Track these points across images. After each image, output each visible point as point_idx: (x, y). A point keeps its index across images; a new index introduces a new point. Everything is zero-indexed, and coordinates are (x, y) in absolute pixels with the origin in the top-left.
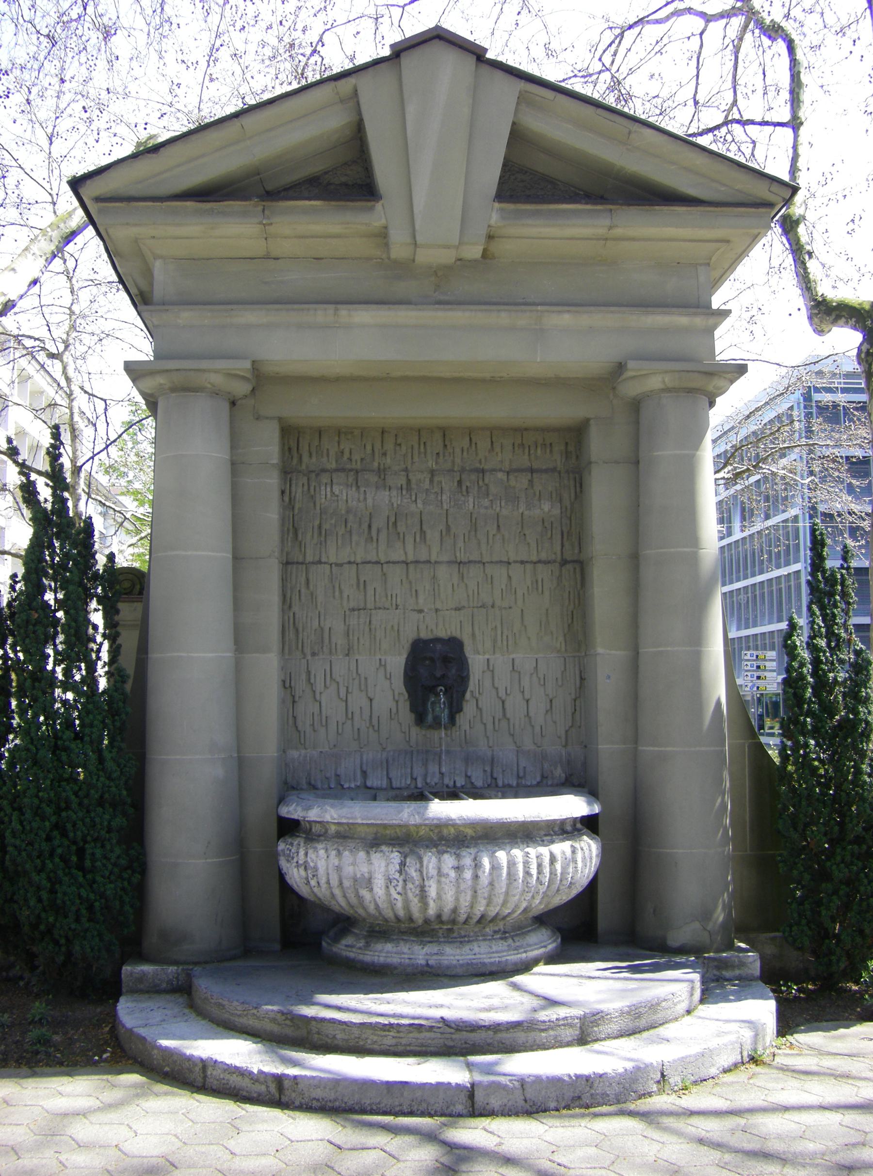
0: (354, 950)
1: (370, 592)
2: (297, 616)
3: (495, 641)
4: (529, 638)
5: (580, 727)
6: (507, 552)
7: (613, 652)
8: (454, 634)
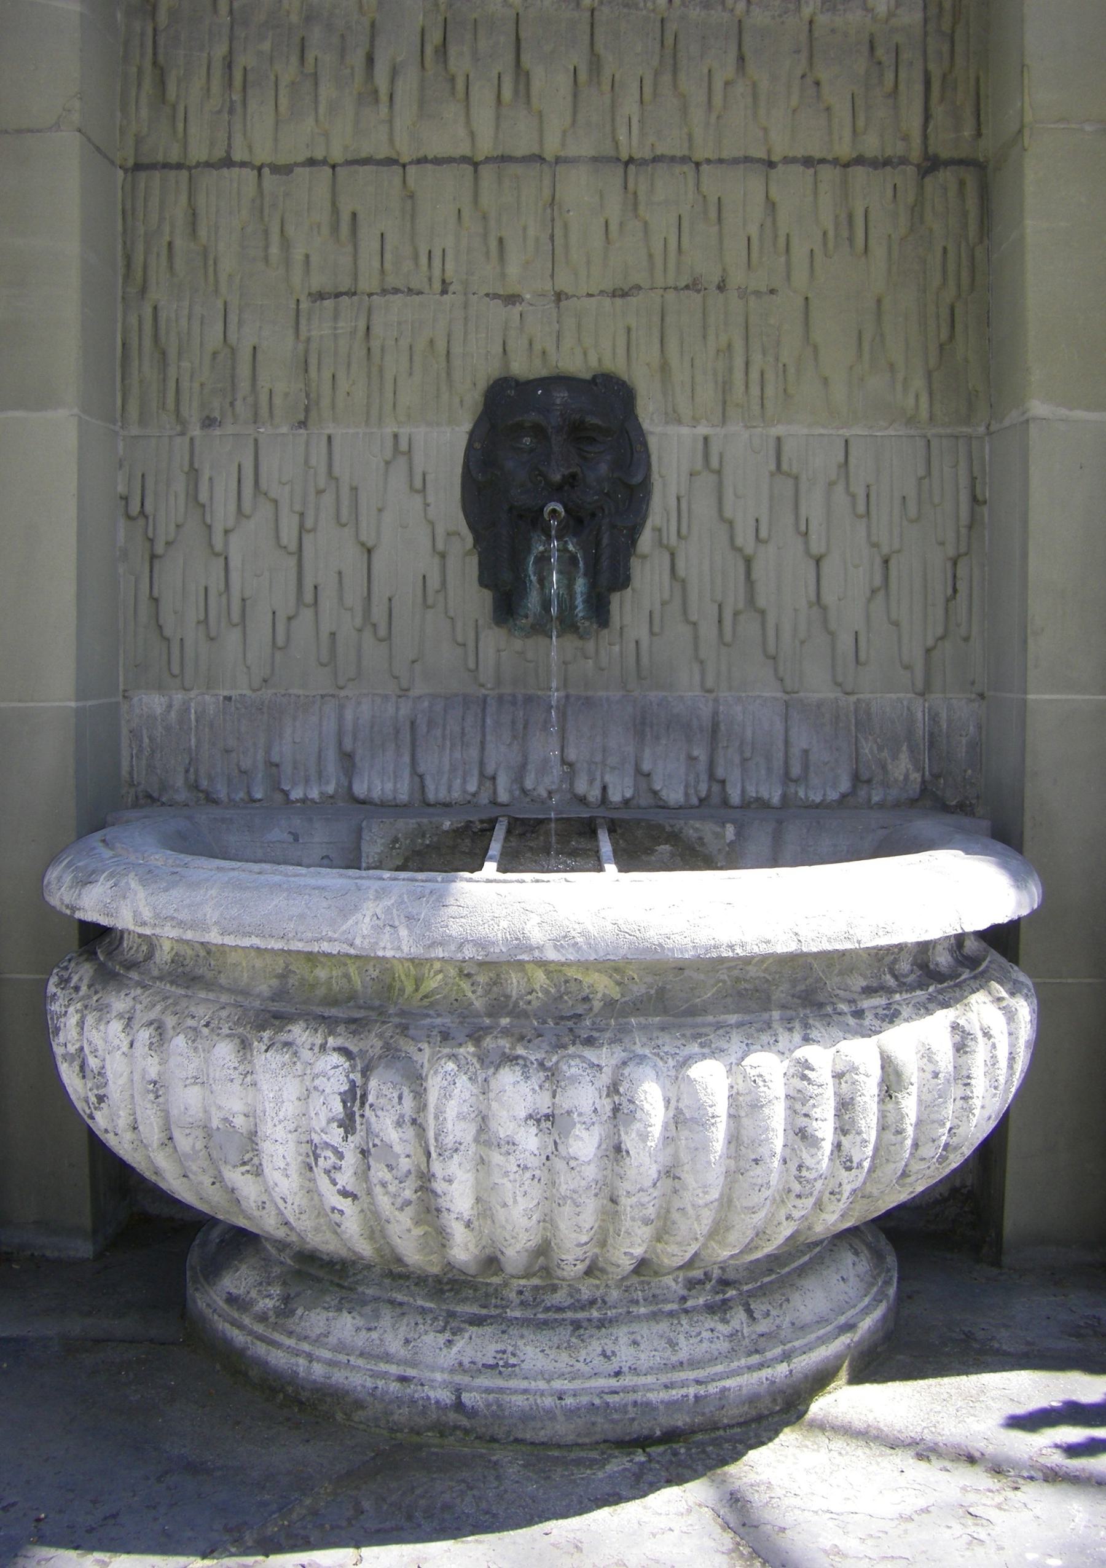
1: (369, 245)
2: (163, 315)
3: (725, 387)
4: (825, 381)
5: (966, 639)
6: (765, 130)
7: (1079, 414)
8: (609, 366)
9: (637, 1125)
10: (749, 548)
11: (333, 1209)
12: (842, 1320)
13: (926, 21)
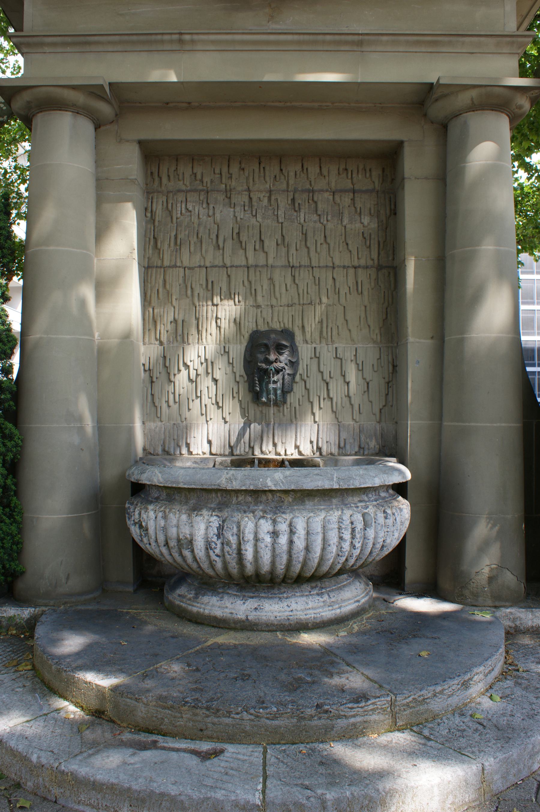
0: (184, 600)
5: (392, 406)
9: (297, 535)
10: (328, 380)
11: (214, 560)
12: (356, 599)
13: (378, 226)
